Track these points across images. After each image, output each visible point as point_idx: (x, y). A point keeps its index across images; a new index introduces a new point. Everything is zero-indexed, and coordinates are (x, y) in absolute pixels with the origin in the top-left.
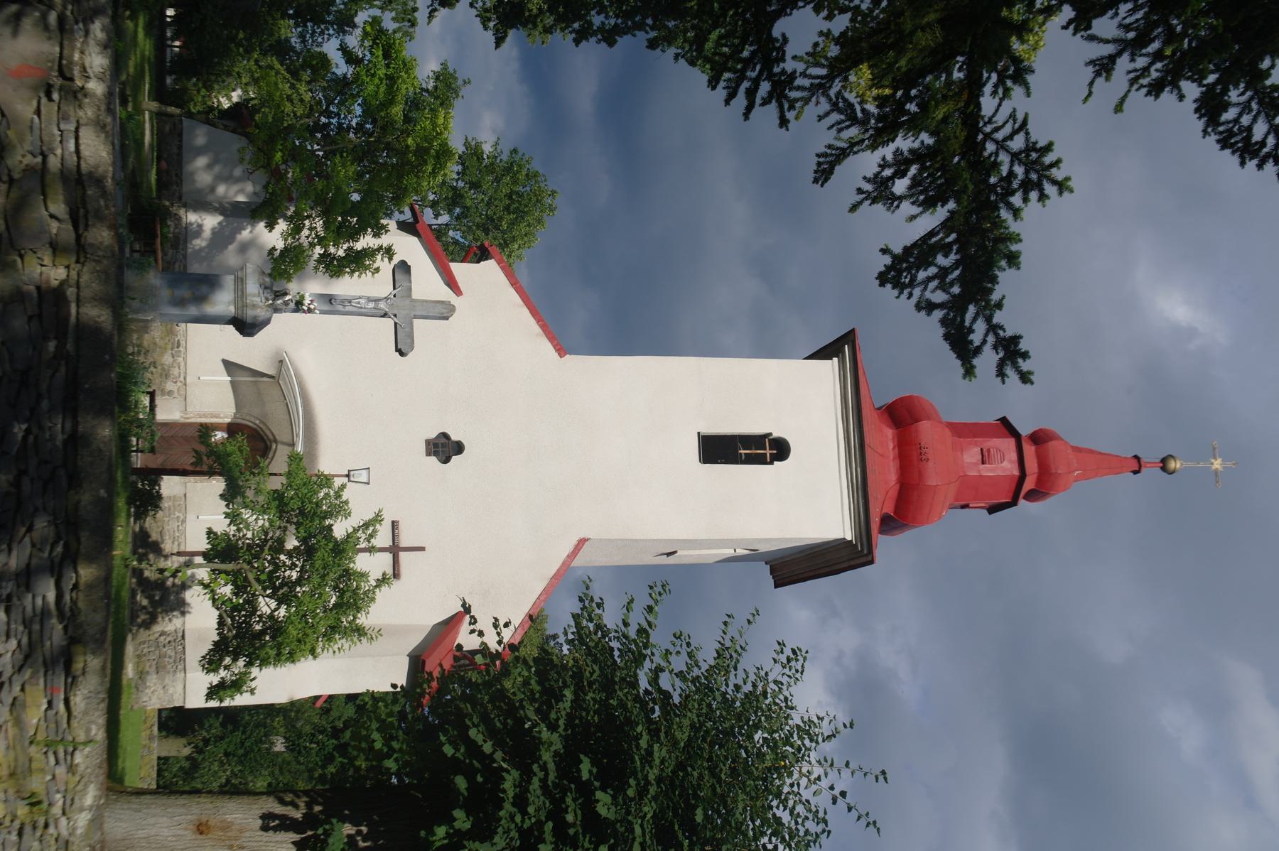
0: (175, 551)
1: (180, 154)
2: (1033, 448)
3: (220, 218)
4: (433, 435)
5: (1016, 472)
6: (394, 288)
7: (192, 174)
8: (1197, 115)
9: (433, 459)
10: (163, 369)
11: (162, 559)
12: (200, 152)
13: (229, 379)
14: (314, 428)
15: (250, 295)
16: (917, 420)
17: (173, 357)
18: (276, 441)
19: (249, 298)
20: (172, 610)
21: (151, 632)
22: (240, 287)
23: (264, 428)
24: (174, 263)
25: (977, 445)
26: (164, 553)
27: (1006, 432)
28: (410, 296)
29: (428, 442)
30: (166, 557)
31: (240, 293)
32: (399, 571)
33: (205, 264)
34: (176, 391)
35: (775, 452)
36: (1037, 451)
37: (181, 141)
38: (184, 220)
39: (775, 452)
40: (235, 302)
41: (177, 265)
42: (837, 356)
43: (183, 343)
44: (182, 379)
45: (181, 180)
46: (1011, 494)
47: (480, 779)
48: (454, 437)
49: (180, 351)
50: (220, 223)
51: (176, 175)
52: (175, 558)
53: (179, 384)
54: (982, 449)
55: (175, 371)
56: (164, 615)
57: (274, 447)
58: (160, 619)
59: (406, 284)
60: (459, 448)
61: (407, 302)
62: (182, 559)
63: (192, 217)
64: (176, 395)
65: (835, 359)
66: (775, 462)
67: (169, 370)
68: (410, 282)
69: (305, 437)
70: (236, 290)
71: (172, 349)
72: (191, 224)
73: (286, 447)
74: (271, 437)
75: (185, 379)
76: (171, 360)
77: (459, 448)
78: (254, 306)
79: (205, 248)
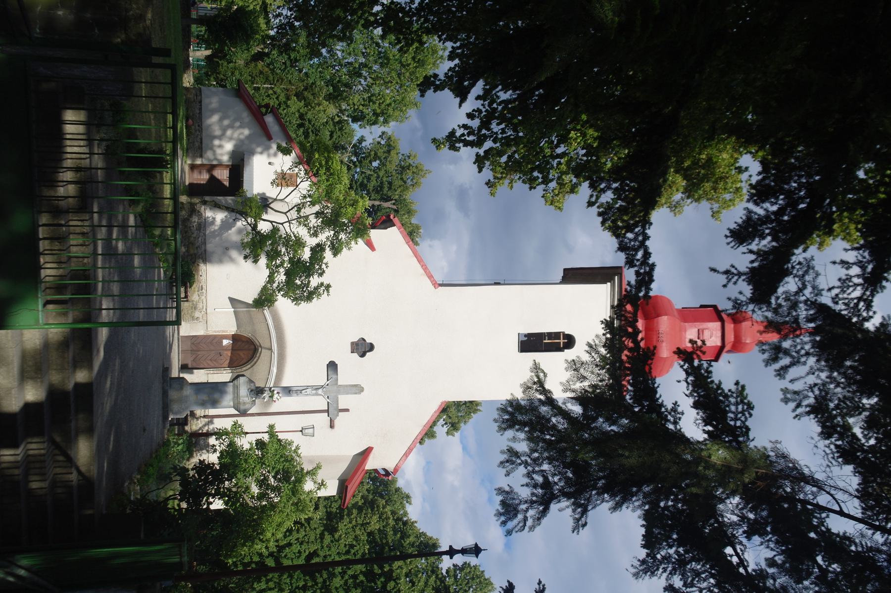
0: (202, 415)
1: (200, 113)
2: (732, 326)
3: (226, 214)
4: (356, 340)
5: (719, 343)
6: (328, 380)
7: (209, 126)
8: (775, 373)
9: (356, 354)
10: (193, 304)
11: (195, 420)
12: (214, 111)
13: (233, 310)
14: (284, 338)
15: (242, 397)
16: (658, 315)
17: (199, 296)
18: (261, 346)
19: (241, 398)
20: (202, 449)
21: (190, 463)
22: (236, 391)
23: (254, 338)
24: (198, 238)
25: (696, 327)
26: (197, 417)
27: (717, 319)
28: (337, 384)
29: (352, 343)
30: (197, 419)
31: (236, 395)
32: (333, 424)
33: (217, 238)
34: (201, 317)
35: (566, 341)
36: (734, 327)
37: (201, 105)
38: (204, 215)
39: (566, 341)
40: (233, 400)
41: (200, 239)
42: (610, 282)
43: (204, 287)
44: (204, 310)
45: (202, 129)
46: (715, 356)
47: (440, 33)
48: (368, 341)
49: (203, 293)
50: (226, 217)
51: (199, 126)
52: (202, 419)
53: (203, 313)
54: (699, 330)
55: (200, 306)
56: (197, 452)
57: (260, 350)
58: (195, 455)
59: (334, 377)
60: (371, 347)
61: (335, 387)
62: (206, 420)
63: (209, 214)
64: (201, 320)
65: (609, 284)
66: (565, 350)
67: (197, 304)
68: (337, 375)
69: (277, 337)
70: (234, 393)
71: (198, 291)
72: (208, 217)
73: (267, 351)
74: (258, 344)
75: (206, 310)
76: (197, 298)
77: (371, 347)
78: (244, 403)
79: (217, 230)
